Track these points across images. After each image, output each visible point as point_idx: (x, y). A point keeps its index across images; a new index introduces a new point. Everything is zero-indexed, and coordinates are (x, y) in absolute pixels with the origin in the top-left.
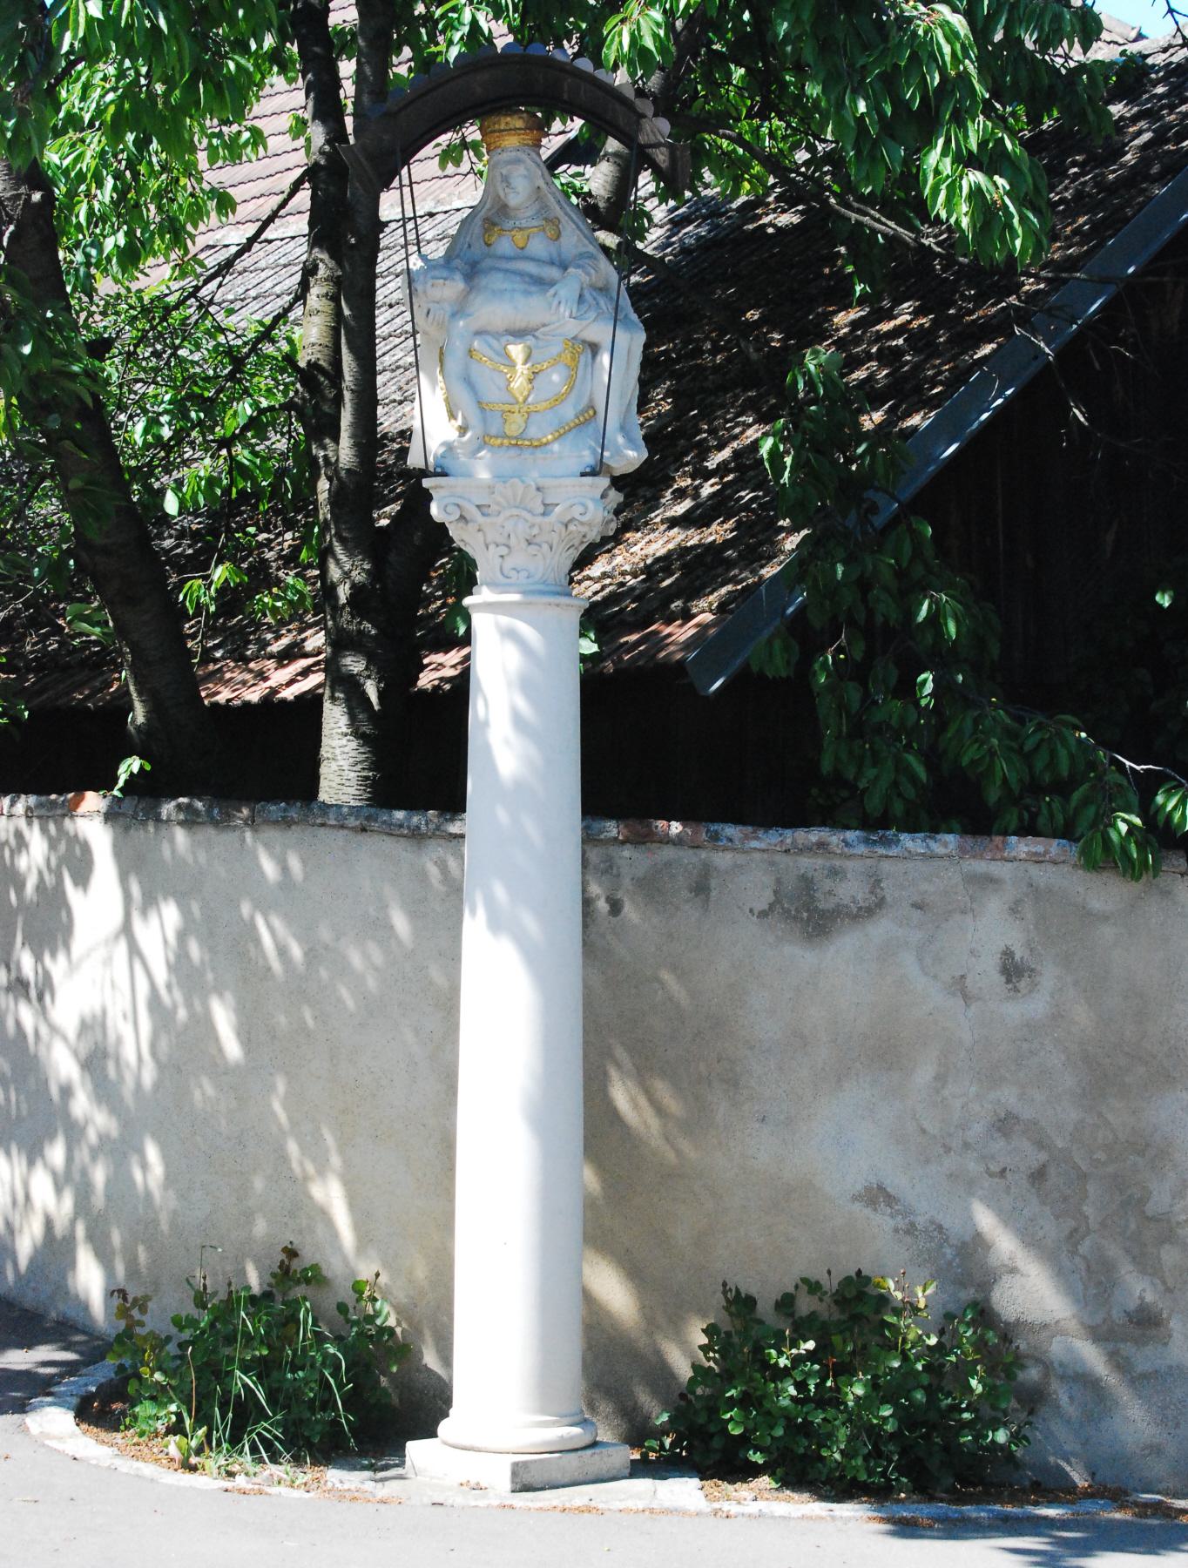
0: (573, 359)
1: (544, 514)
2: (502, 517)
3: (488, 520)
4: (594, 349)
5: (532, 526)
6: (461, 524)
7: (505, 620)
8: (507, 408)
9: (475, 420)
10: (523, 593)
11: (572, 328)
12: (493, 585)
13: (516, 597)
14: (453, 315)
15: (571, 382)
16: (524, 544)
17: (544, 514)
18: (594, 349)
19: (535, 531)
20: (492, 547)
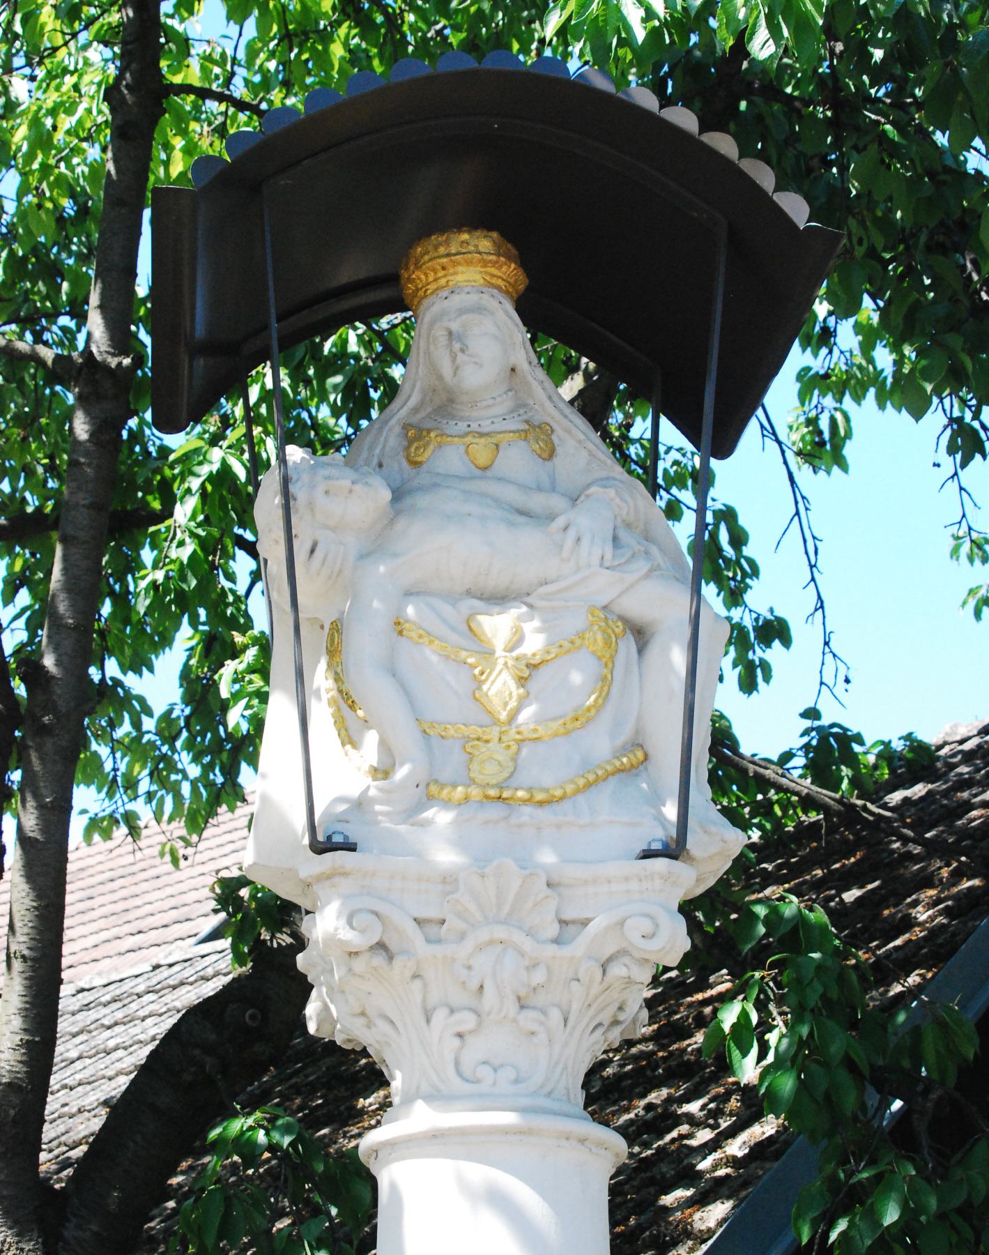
0: (607, 643)
1: (557, 941)
2: (469, 944)
3: (437, 950)
4: (641, 634)
5: (534, 966)
6: (379, 960)
7: (478, 1173)
8: (474, 731)
9: (407, 738)
10: (523, 1110)
11: (605, 586)
12: (436, 1097)
13: (508, 1118)
14: (363, 556)
15: (604, 683)
16: (511, 1007)
17: (557, 941)
18: (641, 634)
19: (539, 977)
20: (440, 1016)
